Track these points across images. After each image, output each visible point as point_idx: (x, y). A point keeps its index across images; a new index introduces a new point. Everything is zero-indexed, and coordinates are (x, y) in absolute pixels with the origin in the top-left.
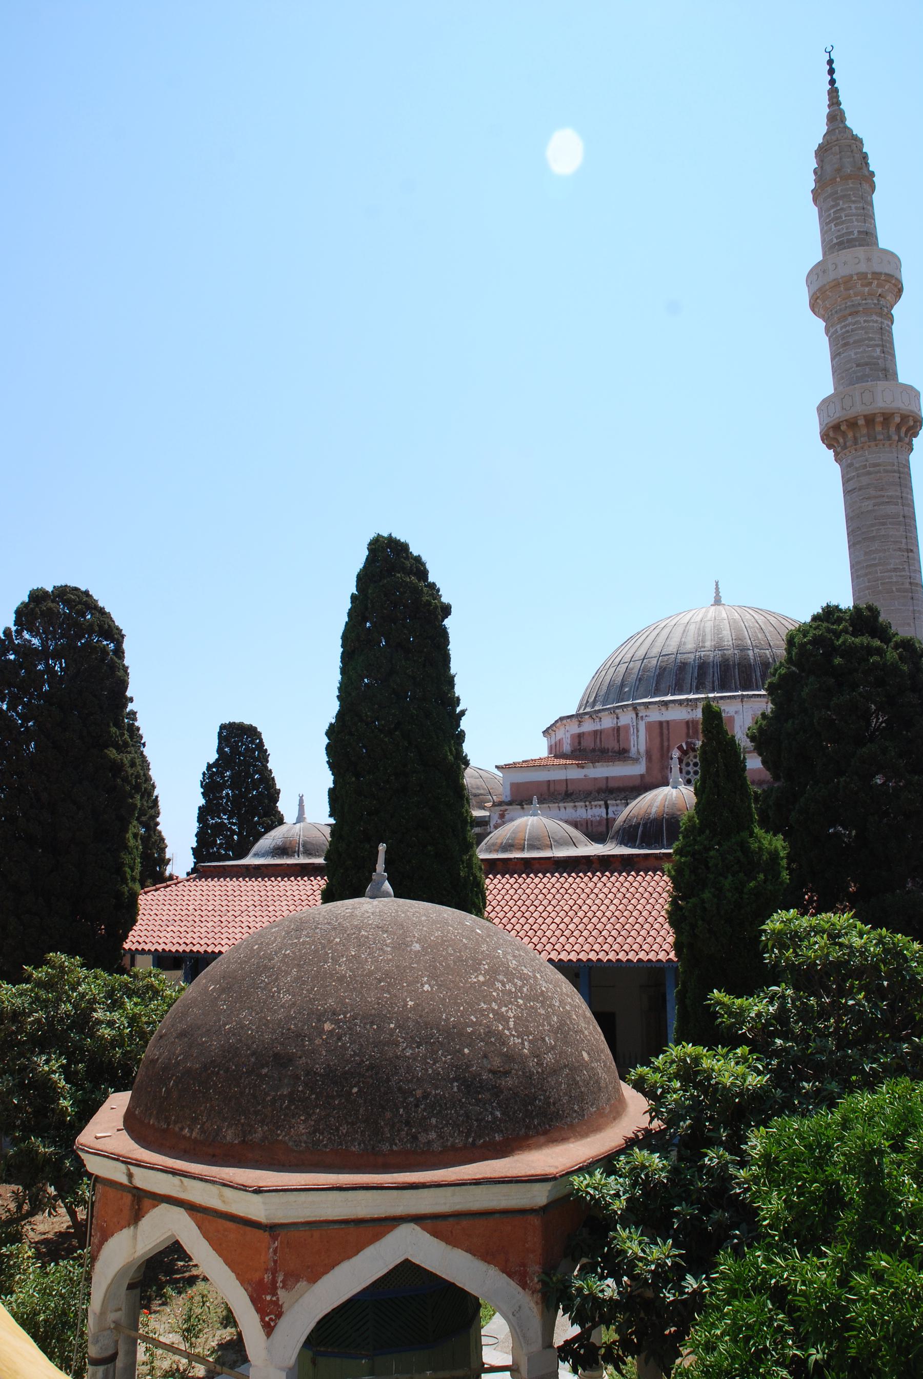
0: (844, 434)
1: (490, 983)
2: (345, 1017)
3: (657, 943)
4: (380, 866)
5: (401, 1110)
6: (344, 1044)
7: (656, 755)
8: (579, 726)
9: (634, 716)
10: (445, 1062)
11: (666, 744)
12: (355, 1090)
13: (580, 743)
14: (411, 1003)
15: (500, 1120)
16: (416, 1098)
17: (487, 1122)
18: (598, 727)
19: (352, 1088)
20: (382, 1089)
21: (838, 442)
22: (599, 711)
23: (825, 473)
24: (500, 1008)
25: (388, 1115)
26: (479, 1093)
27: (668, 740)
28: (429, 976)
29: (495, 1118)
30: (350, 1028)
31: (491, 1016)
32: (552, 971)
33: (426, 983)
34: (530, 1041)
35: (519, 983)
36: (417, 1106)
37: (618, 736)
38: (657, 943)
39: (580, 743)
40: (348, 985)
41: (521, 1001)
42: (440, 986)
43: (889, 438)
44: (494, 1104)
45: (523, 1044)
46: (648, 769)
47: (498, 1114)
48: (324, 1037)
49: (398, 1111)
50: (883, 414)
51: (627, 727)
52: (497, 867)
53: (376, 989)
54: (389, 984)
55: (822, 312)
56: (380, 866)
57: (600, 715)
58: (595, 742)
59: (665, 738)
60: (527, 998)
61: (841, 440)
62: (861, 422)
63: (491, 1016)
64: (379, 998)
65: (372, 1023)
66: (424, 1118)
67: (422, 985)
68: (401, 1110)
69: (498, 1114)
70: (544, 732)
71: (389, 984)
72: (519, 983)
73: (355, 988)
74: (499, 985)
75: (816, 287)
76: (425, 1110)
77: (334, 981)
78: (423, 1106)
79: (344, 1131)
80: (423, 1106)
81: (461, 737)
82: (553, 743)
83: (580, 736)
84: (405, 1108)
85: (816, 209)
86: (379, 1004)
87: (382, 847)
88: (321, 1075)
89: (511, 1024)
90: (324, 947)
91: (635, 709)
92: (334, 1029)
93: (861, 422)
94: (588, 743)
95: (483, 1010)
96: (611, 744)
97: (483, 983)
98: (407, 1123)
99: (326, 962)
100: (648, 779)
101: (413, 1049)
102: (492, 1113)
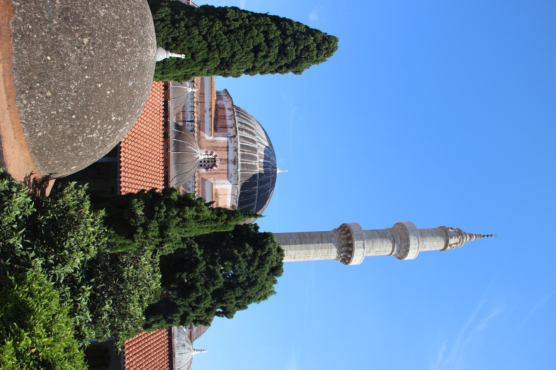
0: (346, 234)
1: (111, 122)
2: (91, 50)
3: (129, 184)
4: (175, 55)
5: (38, 85)
6: (75, 51)
7: (213, 144)
8: (228, 109)
9: (232, 135)
10: (67, 106)
11: (218, 149)
12: (49, 58)
13: (220, 108)
14: (100, 86)
15: (36, 135)
16: (46, 92)
17: (35, 129)
18: (227, 118)
19: (50, 56)
20: (50, 74)
21: (343, 231)
22: (235, 119)
23: (330, 225)
24: (98, 130)
25: (36, 78)
26: (51, 125)
27: (220, 151)
28: (114, 93)
29: (38, 133)
30: (85, 54)
31: (94, 126)
32: (115, 143)
33: (111, 92)
34: (80, 145)
35: (111, 136)
36: (41, 93)
37: (223, 127)
38: (129, 184)
39: (220, 108)
40: (109, 50)
41: (101, 138)
42: (109, 99)
43: (342, 252)
44: (45, 132)
45: (79, 142)
46: (208, 141)
47: (40, 134)
48: (79, 39)
49: (38, 83)
50: (352, 251)
51: (226, 132)
52: (166, 87)
53: (108, 66)
54: (110, 73)
55: (397, 227)
56: (175, 55)
57: (233, 119)
58: (221, 116)
59: (221, 149)
60: (103, 141)
61: (343, 232)
62: (350, 242)
63: (94, 126)
64: (102, 68)
65: (88, 66)
66: (35, 97)
67: (110, 90)
68: (38, 85)
69: (40, 134)
70: (226, 90)
71: (110, 73)
72: (111, 136)
73: (108, 54)
74: (110, 127)
75: (407, 226)
76: (39, 97)
77: (112, 41)
78: (41, 96)
79: (24, 52)
80: (41, 96)
81: (220, 7)
82: (221, 94)
83: (224, 109)
84: (40, 86)
85: (437, 227)
86: (99, 69)
87: (183, 56)
88: (57, 38)
89: (90, 136)
90: (131, 33)
91: (234, 136)
92: (84, 44)
93: (349, 234)
94: (220, 113)
95: (96, 122)
96: (220, 123)
97: (111, 120)
98: (31, 88)
99: (123, 35)
100: (202, 140)
101: (75, 88)
102: (40, 131)
